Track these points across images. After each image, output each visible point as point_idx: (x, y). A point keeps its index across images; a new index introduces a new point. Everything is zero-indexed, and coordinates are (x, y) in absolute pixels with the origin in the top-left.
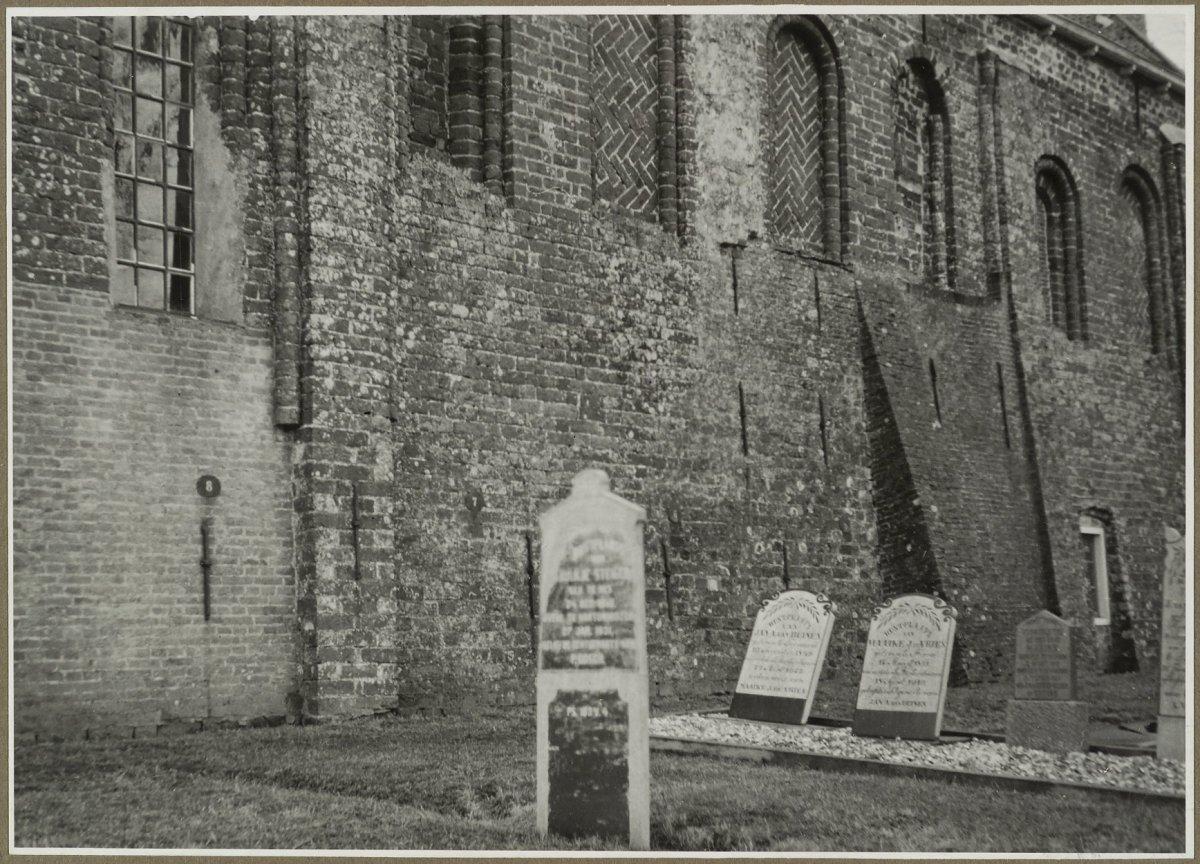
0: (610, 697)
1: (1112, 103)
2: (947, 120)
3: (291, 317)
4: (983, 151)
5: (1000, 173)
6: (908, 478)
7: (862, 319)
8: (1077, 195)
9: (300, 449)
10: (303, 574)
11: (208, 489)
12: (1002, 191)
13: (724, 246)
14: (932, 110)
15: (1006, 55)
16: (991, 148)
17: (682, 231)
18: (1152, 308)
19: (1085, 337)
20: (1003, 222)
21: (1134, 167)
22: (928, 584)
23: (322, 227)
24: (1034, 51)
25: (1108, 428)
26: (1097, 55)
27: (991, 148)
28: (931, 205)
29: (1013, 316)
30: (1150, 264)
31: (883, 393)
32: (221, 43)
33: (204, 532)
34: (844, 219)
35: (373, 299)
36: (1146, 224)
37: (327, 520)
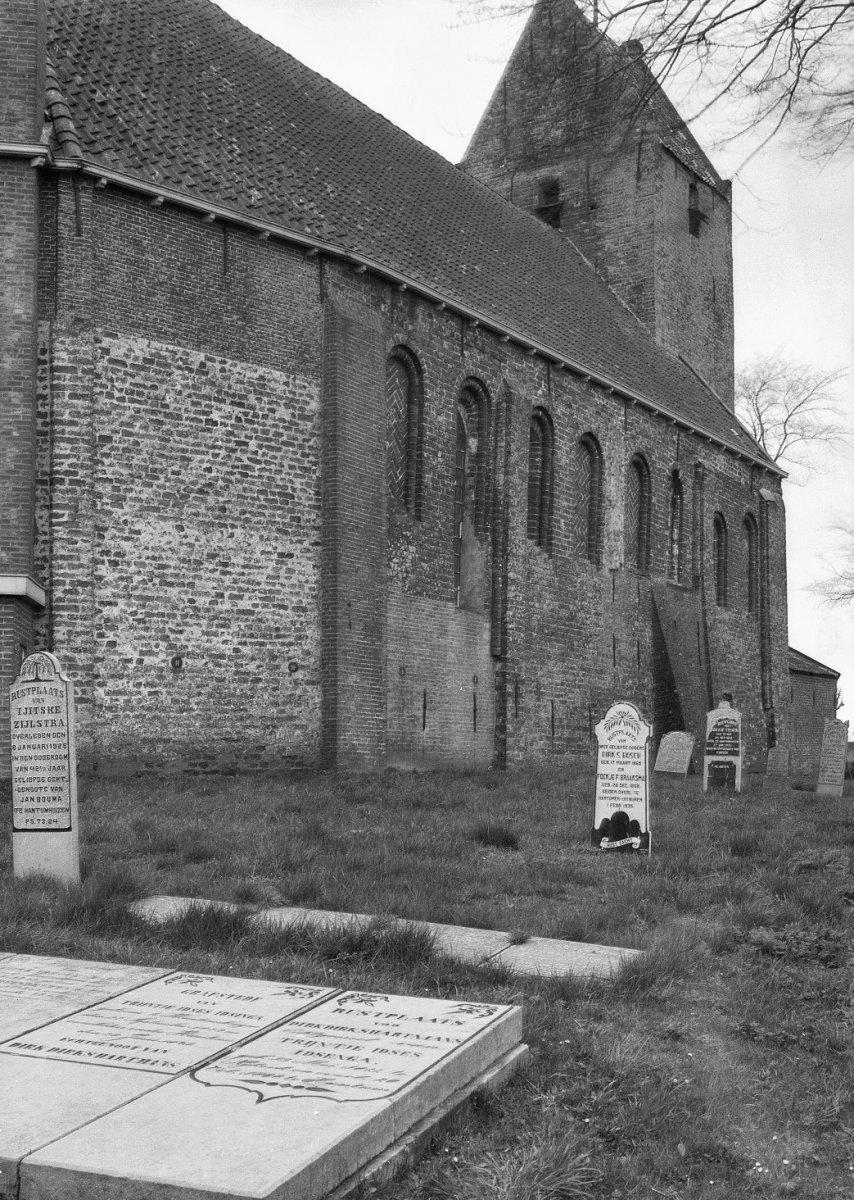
0: (730, 763)
1: (742, 481)
2: (682, 499)
3: (500, 611)
4: (695, 512)
5: (702, 525)
6: (673, 679)
7: (654, 602)
8: (726, 531)
9: (499, 665)
10: (499, 715)
11: (475, 681)
12: (702, 535)
13: (611, 570)
14: (675, 493)
15: (706, 463)
16: (699, 512)
17: (598, 563)
18: (750, 587)
19: (725, 605)
20: (702, 550)
21: (750, 514)
22: (681, 727)
23: (511, 575)
24: (715, 459)
25: (732, 653)
26: (406, 290)
27: (699, 512)
28: (673, 541)
29: (704, 598)
30: (750, 564)
31: (663, 639)
32: (476, 496)
33: (475, 698)
34: (648, 553)
35: (522, 604)
36: (750, 542)
37: (510, 694)
